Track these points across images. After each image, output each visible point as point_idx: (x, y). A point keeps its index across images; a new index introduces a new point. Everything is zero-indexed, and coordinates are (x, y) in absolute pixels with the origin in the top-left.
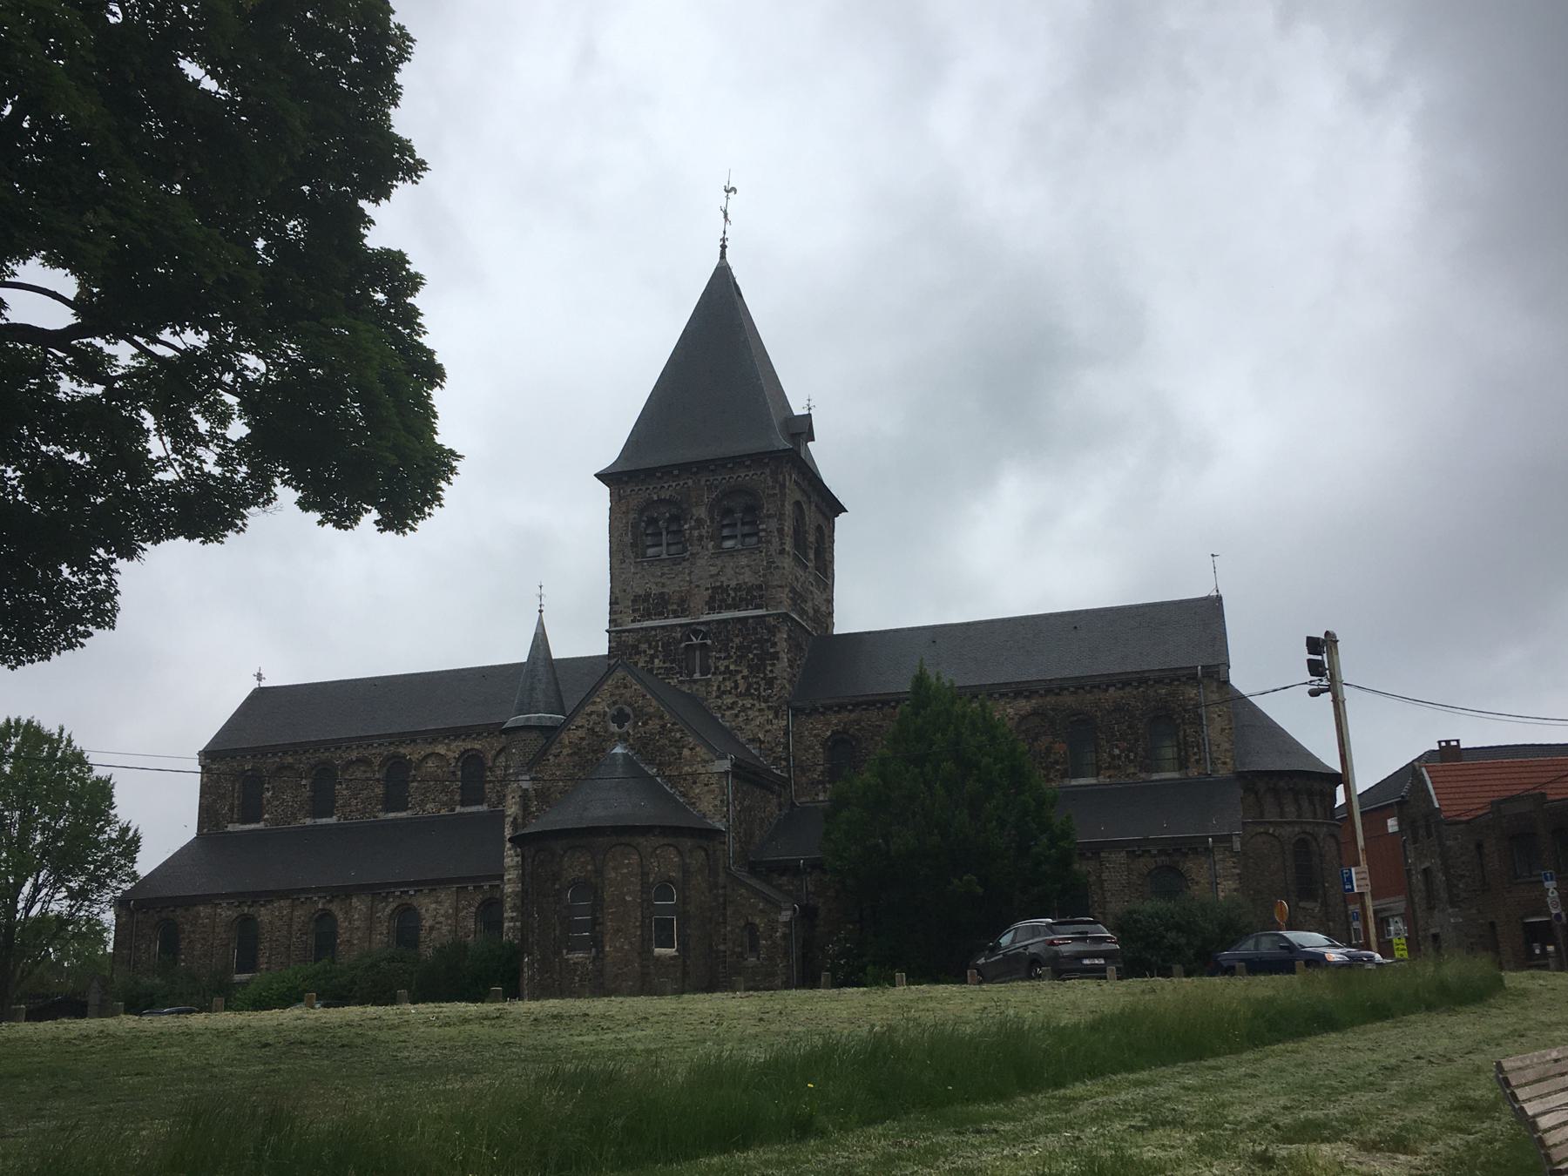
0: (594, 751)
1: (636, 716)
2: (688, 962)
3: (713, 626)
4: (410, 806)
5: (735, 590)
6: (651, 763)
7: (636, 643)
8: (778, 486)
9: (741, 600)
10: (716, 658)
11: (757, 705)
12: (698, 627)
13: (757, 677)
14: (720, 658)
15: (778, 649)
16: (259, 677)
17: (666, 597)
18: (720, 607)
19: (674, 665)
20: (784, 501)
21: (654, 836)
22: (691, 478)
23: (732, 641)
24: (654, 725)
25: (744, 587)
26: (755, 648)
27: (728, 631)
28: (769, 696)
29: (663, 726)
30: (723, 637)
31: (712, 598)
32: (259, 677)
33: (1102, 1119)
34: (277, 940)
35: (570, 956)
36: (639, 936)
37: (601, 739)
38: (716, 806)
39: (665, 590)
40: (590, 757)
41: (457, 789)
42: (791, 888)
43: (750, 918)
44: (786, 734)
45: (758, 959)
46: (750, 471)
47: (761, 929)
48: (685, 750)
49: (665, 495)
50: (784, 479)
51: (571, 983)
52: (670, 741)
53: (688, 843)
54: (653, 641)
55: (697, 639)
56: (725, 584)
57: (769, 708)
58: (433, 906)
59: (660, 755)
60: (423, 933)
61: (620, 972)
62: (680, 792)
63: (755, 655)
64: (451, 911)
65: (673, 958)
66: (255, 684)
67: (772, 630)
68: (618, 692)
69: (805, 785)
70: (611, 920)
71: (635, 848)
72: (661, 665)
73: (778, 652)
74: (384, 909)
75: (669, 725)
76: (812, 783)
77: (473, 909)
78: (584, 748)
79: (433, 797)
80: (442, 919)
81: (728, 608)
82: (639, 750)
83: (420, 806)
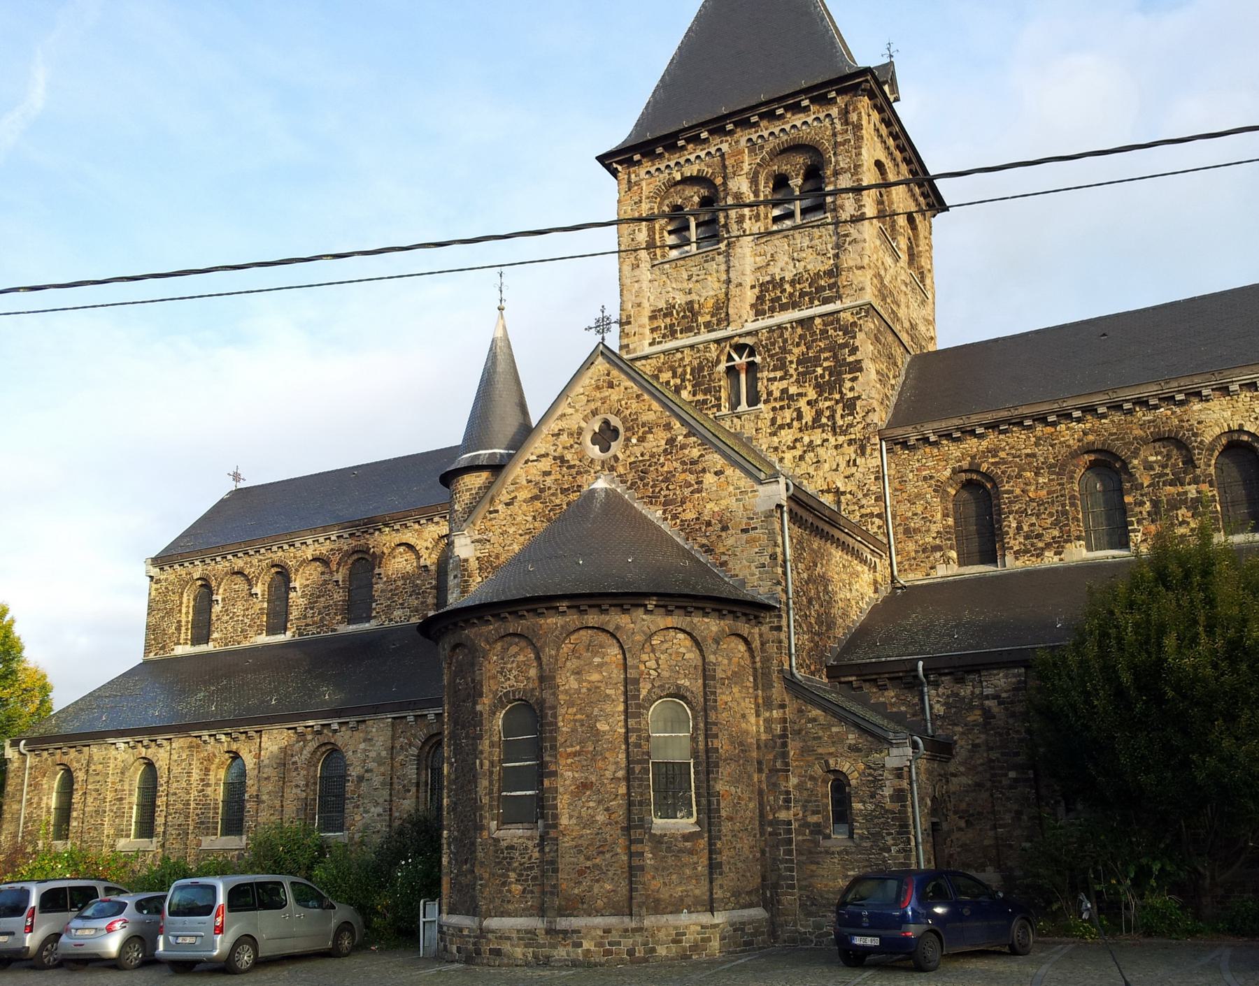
0: (564, 491)
1: (627, 429)
2: (719, 844)
3: (764, 335)
4: (374, 614)
5: (792, 283)
6: (652, 500)
7: (656, 373)
8: (850, 127)
9: (802, 294)
10: (769, 380)
11: (832, 440)
12: (742, 341)
13: (831, 399)
14: (774, 379)
15: (859, 356)
16: (236, 477)
17: (696, 306)
18: (772, 310)
19: (709, 397)
20: (860, 147)
21: (647, 612)
22: (727, 141)
23: (790, 352)
24: (656, 441)
25: (806, 276)
26: (826, 359)
27: (785, 341)
28: (850, 425)
29: (671, 442)
30: (777, 350)
31: (760, 298)
32: (236, 477)
33: (994, 827)
34: (175, 794)
35: (501, 834)
36: (623, 795)
37: (574, 471)
38: (763, 566)
39: (694, 297)
40: (558, 502)
41: (431, 588)
42: (903, 709)
43: (832, 762)
44: (879, 477)
45: (851, 836)
46: (809, 116)
47: (853, 782)
48: (708, 475)
49: (692, 170)
50: (860, 118)
51: (504, 884)
52: (683, 463)
53: (710, 625)
54: (680, 366)
55: (741, 358)
56: (778, 278)
57: (850, 442)
58: (362, 746)
59: (668, 489)
60: (350, 786)
61: (589, 864)
62: (702, 546)
63: (825, 369)
64: (384, 753)
65: (687, 837)
66: (231, 486)
67: (849, 330)
68: (598, 395)
69: (913, 554)
70: (570, 767)
71: (613, 635)
72: (691, 398)
73: (860, 361)
74: (302, 750)
75: (680, 438)
76: (924, 551)
77: (414, 751)
78: (549, 488)
79: (401, 601)
80: (372, 765)
81: (783, 308)
82: (633, 484)
83: (385, 614)
